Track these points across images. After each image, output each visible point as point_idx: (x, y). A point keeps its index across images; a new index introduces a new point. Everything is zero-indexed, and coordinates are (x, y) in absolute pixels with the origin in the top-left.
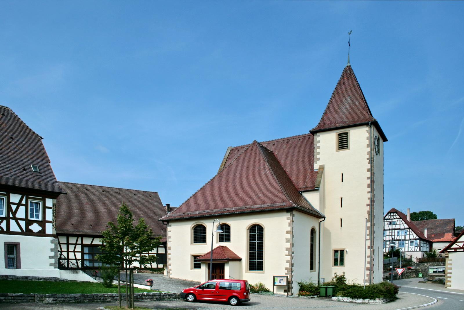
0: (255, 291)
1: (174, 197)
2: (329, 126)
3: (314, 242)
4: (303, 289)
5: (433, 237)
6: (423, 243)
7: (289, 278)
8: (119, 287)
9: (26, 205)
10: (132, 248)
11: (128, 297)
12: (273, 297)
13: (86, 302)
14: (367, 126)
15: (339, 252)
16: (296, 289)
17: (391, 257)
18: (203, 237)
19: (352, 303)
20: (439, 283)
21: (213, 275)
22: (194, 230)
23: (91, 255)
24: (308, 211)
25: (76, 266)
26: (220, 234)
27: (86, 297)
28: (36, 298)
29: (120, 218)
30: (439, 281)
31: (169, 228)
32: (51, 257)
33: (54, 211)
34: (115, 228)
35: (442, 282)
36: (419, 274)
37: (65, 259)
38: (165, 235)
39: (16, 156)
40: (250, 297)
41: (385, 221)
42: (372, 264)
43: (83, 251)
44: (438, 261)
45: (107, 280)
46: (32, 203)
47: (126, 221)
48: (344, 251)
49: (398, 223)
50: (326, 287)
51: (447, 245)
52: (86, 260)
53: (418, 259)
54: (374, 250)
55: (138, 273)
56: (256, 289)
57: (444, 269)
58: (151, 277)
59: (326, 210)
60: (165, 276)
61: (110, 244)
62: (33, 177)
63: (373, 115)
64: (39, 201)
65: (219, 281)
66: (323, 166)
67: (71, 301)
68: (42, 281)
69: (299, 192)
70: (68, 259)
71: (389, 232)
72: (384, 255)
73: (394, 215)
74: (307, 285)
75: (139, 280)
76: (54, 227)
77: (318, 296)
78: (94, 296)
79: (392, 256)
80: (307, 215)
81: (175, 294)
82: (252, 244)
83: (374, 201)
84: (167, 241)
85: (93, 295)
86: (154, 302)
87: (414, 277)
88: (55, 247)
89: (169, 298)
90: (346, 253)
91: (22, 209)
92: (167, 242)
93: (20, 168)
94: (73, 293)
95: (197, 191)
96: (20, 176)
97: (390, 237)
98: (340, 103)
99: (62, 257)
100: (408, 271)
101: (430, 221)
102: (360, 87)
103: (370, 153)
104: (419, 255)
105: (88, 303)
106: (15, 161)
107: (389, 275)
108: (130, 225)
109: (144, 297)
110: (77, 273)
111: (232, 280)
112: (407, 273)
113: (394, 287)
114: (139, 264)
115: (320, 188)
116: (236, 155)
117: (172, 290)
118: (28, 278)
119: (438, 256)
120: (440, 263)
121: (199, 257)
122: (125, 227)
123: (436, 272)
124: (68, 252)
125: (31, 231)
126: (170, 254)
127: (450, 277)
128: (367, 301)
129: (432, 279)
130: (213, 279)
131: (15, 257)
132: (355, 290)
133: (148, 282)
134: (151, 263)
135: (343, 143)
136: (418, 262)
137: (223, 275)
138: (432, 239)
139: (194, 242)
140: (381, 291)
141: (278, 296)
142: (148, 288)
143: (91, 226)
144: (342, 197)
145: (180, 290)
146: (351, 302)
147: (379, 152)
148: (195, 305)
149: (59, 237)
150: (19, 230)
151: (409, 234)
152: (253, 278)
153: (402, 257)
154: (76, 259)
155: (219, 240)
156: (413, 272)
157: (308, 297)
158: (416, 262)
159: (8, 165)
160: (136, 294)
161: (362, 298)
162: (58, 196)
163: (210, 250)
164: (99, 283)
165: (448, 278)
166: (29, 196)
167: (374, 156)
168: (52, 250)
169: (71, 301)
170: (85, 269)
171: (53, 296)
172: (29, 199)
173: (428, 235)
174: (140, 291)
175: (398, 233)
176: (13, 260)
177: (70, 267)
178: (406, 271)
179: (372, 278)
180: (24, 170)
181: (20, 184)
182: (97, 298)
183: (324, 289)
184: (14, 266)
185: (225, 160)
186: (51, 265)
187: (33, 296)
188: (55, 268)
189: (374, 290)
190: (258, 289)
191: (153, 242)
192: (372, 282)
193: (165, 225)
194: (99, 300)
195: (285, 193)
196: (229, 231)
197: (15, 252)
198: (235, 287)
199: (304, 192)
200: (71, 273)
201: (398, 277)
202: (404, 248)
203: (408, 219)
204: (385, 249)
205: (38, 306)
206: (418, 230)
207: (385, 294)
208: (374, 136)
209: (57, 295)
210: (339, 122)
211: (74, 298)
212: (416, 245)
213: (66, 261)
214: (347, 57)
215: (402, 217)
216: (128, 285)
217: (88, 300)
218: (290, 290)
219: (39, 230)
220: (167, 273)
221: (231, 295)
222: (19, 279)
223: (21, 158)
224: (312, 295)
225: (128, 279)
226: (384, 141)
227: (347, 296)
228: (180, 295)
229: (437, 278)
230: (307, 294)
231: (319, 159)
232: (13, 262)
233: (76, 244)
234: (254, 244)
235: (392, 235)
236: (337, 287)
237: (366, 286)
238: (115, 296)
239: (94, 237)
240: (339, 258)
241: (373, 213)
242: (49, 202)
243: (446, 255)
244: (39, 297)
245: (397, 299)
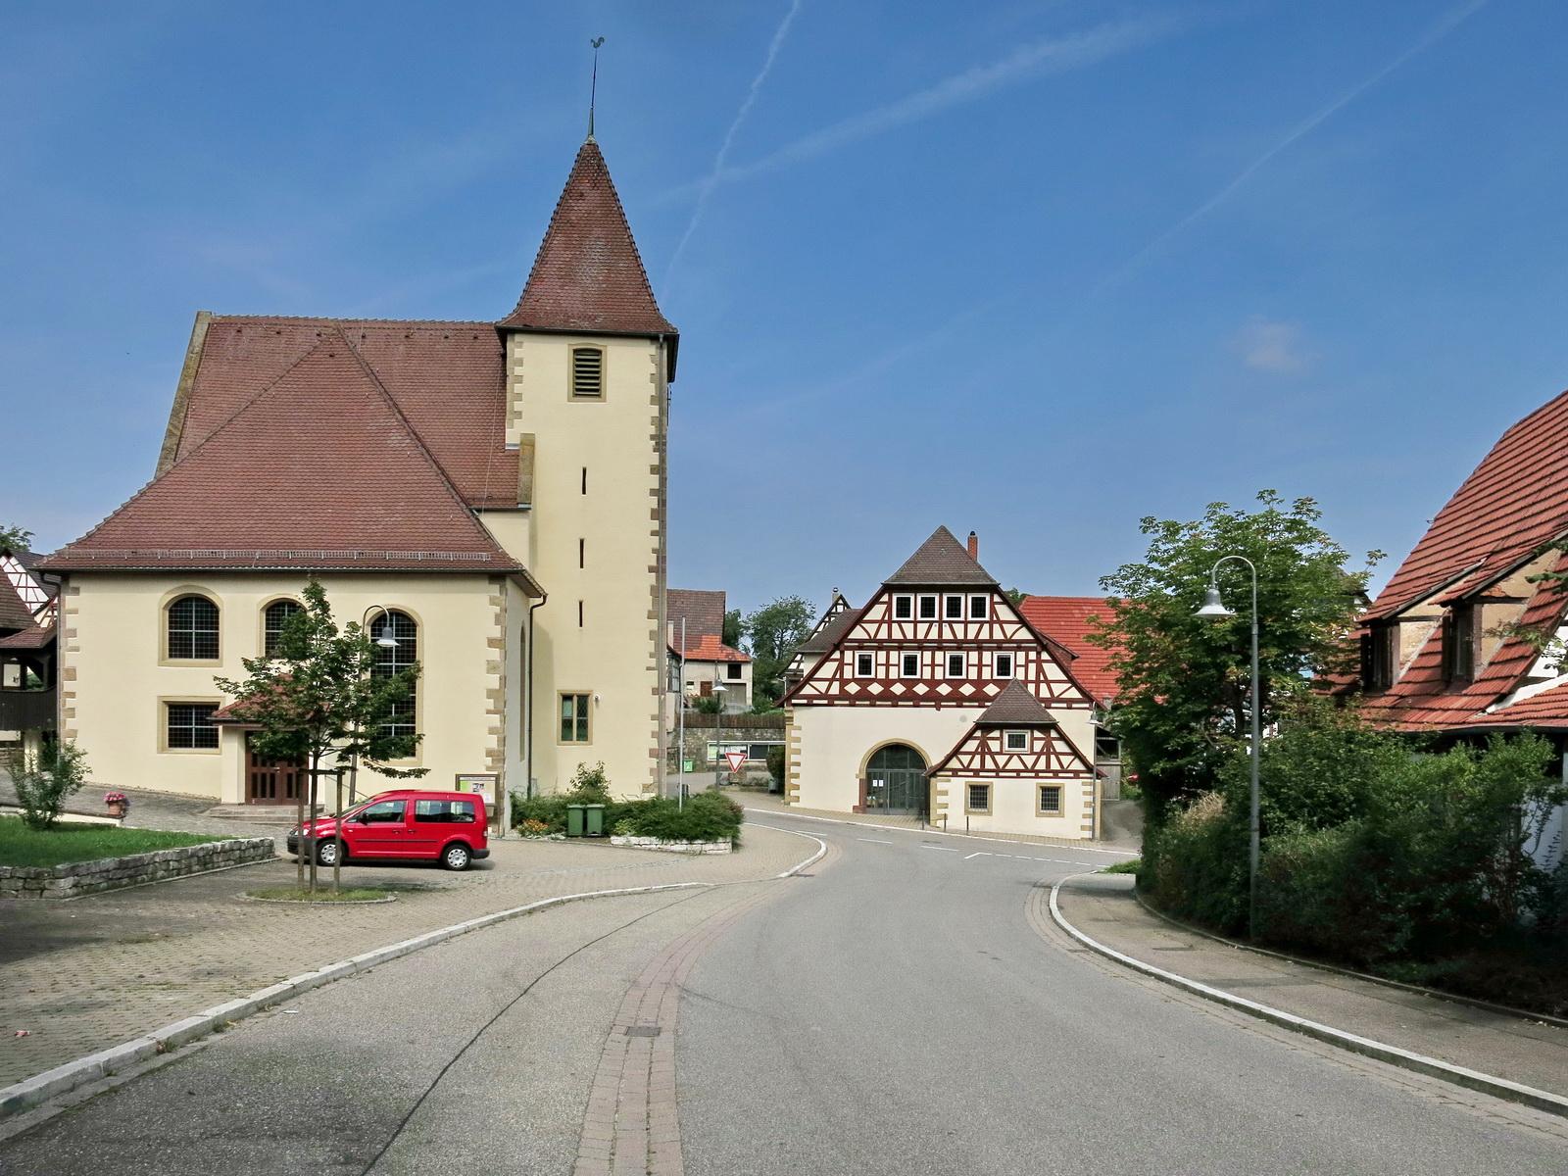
14: (652, 344)
15: (575, 699)
18: (207, 640)
20: (758, 791)
30: (756, 784)
90: (594, 703)
127: (797, 776)
128: (698, 845)
135: (587, 380)
137: (255, 770)
139: (171, 656)
161: (688, 839)
183: (581, 813)
199: (487, 510)
210: (575, 313)
227: (648, 834)
231: (519, 415)
240: (577, 720)
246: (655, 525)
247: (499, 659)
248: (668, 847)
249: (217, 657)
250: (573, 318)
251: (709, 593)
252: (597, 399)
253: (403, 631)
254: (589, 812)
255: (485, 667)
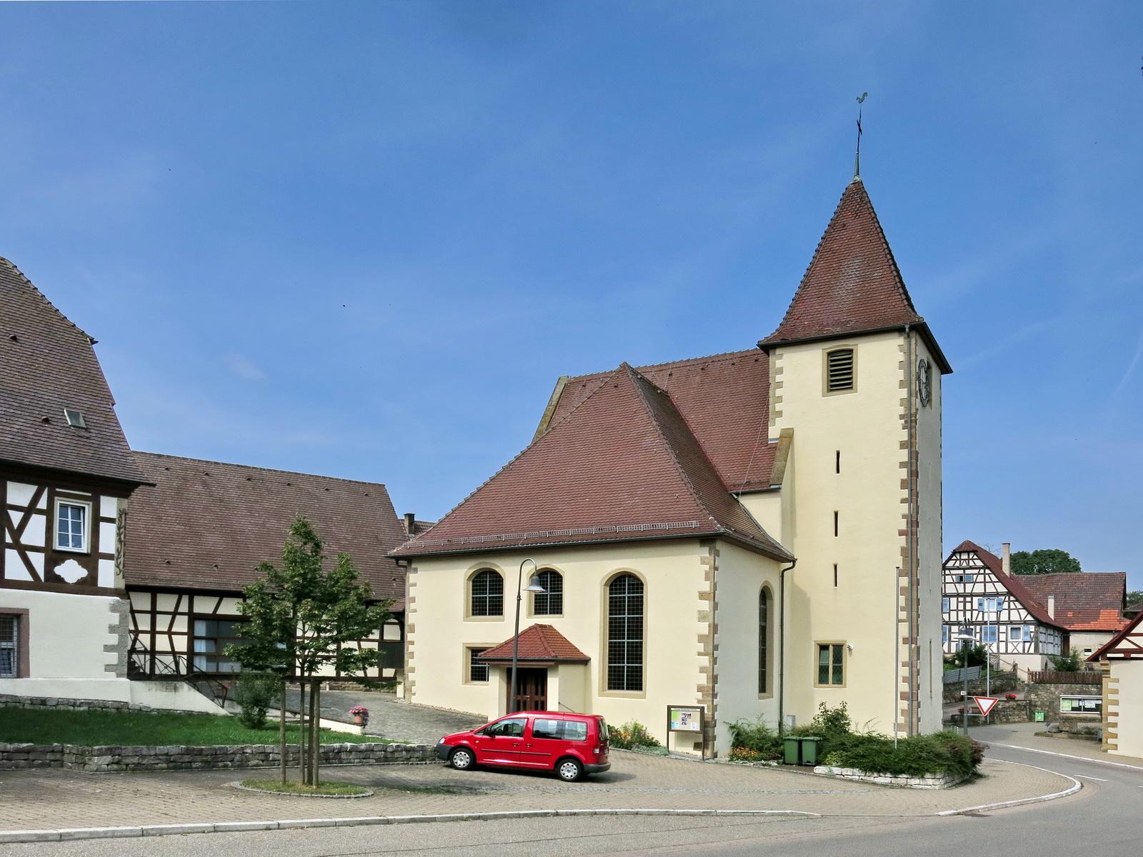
0: (622, 744)
1: (427, 497)
2: (805, 332)
3: (767, 622)
4: (742, 742)
5: (1070, 618)
6: (1045, 634)
7: (706, 711)
8: (282, 729)
9: (49, 513)
10: (319, 630)
11: (304, 757)
12: (666, 761)
13: (196, 768)
15: (831, 648)
16: (723, 741)
17: (963, 666)
19: (865, 785)
20: (1087, 739)
21: (519, 698)
22: (473, 582)
23: (213, 642)
24: (753, 543)
25: (174, 671)
26: (536, 595)
27: (196, 755)
28: (66, 756)
29: (291, 553)
30: (1086, 733)
31: (412, 578)
32: (108, 648)
33: (122, 530)
34: (276, 578)
35: (1093, 737)
36: (1036, 713)
37: (145, 652)
38: (402, 594)
39: (26, 385)
40: (609, 760)
41: (947, 572)
42: (915, 683)
43: (193, 633)
44: (1084, 681)
45: (252, 707)
46: (63, 507)
47: (304, 560)
48: (844, 647)
49: (981, 578)
50: (798, 738)
51: (1107, 639)
52: (199, 654)
53: (1031, 674)
54: (918, 648)
55: (330, 689)
56: (625, 737)
57: (1099, 702)
58: (364, 700)
59: (798, 541)
60: (400, 698)
61: (262, 618)
62: (69, 440)
63: (915, 308)
64: (84, 502)
65: (532, 716)
66: (791, 431)
67: (156, 766)
68: (84, 711)
69: (731, 494)
70: (153, 652)
71: (958, 602)
72: (946, 661)
73: (969, 559)
74: (751, 732)
75: (332, 709)
76: (120, 572)
77: (778, 763)
78: (218, 752)
79: (966, 664)
80: (739, 548)
81: (423, 748)
82: (616, 623)
83: (918, 523)
84: (406, 608)
85: (215, 748)
86: (370, 769)
87: (1023, 721)
88: (120, 622)
89: (408, 759)
91: (37, 524)
92: (406, 613)
93: (35, 415)
94: (163, 743)
95: (482, 485)
96: (34, 437)
97: (961, 613)
98: (833, 277)
99: (136, 647)
100: (1007, 704)
101: (1062, 577)
102: (884, 237)
103: (907, 403)
104: (1034, 663)
105: (202, 769)
106: (22, 398)
107: (959, 713)
108: (315, 570)
109: (343, 756)
110: (176, 689)
111: (564, 715)
112: (1004, 709)
113: (971, 745)
114: (336, 669)
115: (782, 486)
116: (578, 398)
117: (416, 736)
118: (47, 703)
119: (1083, 668)
120: (1090, 686)
121: (485, 652)
122: (304, 576)
123: (1078, 709)
124: (153, 632)
125: (59, 579)
126: (412, 643)
127: (1115, 725)
128: (902, 779)
129: (1067, 729)
130: (518, 710)
131: (16, 648)
132: (872, 749)
133: (355, 714)
134: (364, 669)
135: (840, 376)
136: (1032, 681)
137: (542, 698)
138: (1066, 624)
139: (473, 614)
140: (938, 756)
141: (681, 758)
142: (356, 730)
143: (215, 566)
144: (836, 510)
145: (434, 737)
146: (863, 782)
147: (929, 401)
148: (473, 779)
149: (132, 594)
150: (29, 578)
151: (1009, 609)
152: (618, 711)
153: (991, 666)
154: (173, 653)
155: (535, 610)
156: (1020, 708)
157: (755, 762)
158: (1026, 682)
159: (4, 409)
160: (324, 747)
161: (891, 773)
162: (132, 490)
163: (512, 634)
164: (231, 717)
165: (1108, 727)
166: (57, 490)
167: (917, 409)
168: (112, 629)
169: (157, 764)
170: (195, 679)
171: (110, 752)
172: (56, 498)
173: (1056, 612)
174: (334, 738)
175: (980, 604)
176: (9, 654)
177: (157, 672)
178: (1001, 703)
179: (915, 720)
180: (46, 421)
181: (33, 459)
182: (225, 756)
183: (796, 745)
184: (10, 669)
185: (552, 408)
186: (108, 668)
187: (61, 750)
188: (118, 676)
189: (921, 752)
190: (629, 737)
191: (371, 614)
192: (915, 730)
193: (402, 568)
194: (230, 764)
195: (696, 496)
196: (558, 588)
197: (15, 634)
198: (574, 733)
199: (744, 494)
200: (161, 691)
201: (983, 719)
202: (995, 645)
203: (1006, 569)
204: (946, 645)
205: (72, 778)
206: (1032, 600)
207: (949, 763)
208: (916, 361)
209: (121, 749)
211: (164, 757)
212: (1028, 638)
213: (148, 657)
214: (854, 161)
215: (991, 564)
216: (306, 721)
217: (202, 761)
218: (710, 743)
219: (79, 578)
220: (405, 691)
221: (561, 755)
222: (24, 705)
223: (38, 392)
224: (765, 760)
225: (307, 706)
226: (942, 373)
227: (852, 766)
228: (435, 751)
229: (1081, 725)
230: (751, 756)
231: (780, 414)
232: (9, 659)
233: (175, 614)
234: (619, 671)
235: (965, 610)
236: (827, 740)
237: (899, 742)
238: (270, 753)
239: (221, 594)
240: (832, 664)
241: (914, 554)
242: (109, 506)
243: (1104, 668)
244: (74, 754)
245: (980, 776)
246: (905, 493)
247: (708, 610)
248: (872, 779)
249: (561, 613)
250: (828, 326)
251: (1109, 574)
252: (850, 391)
253: (633, 589)
254: (804, 744)
255: (696, 616)
